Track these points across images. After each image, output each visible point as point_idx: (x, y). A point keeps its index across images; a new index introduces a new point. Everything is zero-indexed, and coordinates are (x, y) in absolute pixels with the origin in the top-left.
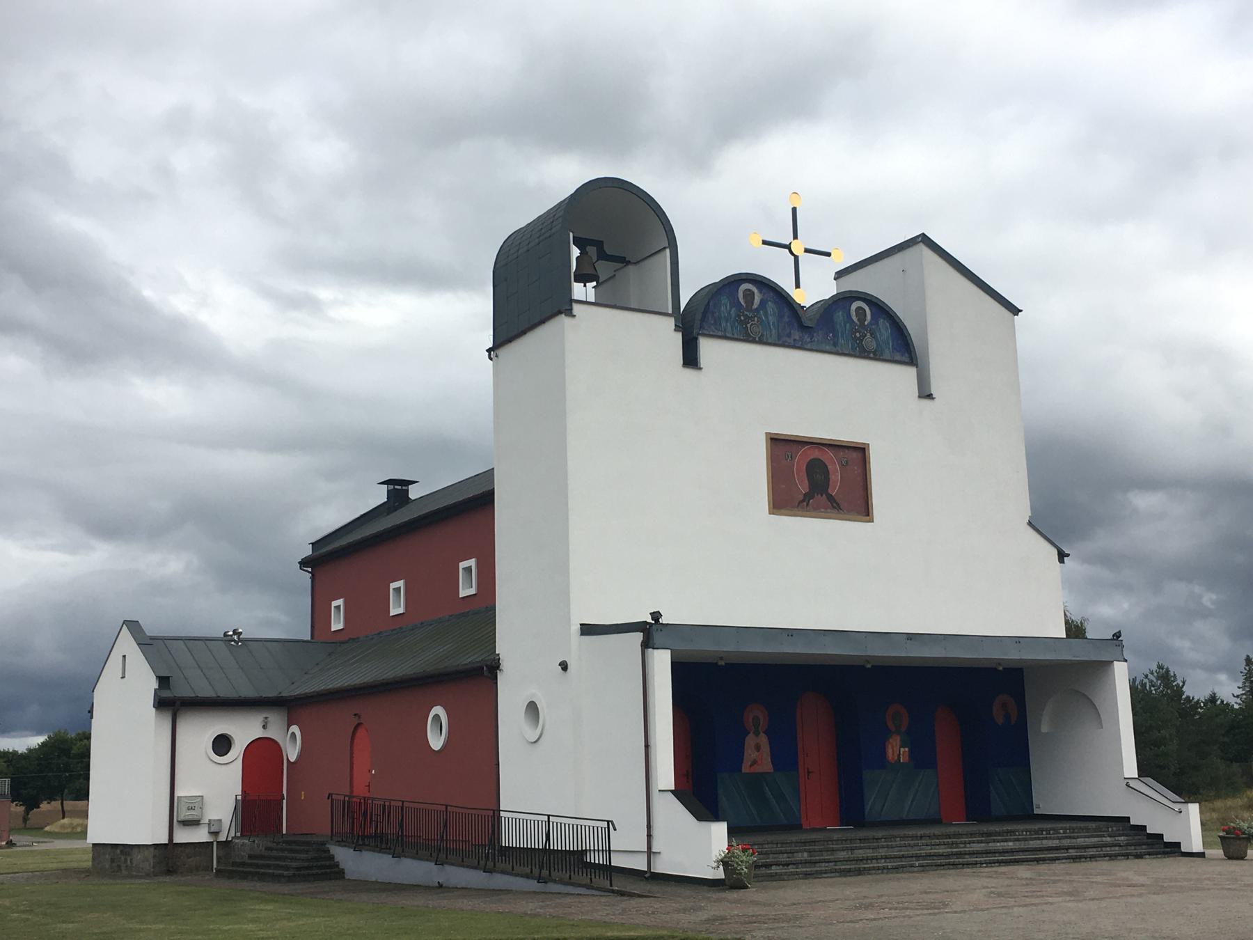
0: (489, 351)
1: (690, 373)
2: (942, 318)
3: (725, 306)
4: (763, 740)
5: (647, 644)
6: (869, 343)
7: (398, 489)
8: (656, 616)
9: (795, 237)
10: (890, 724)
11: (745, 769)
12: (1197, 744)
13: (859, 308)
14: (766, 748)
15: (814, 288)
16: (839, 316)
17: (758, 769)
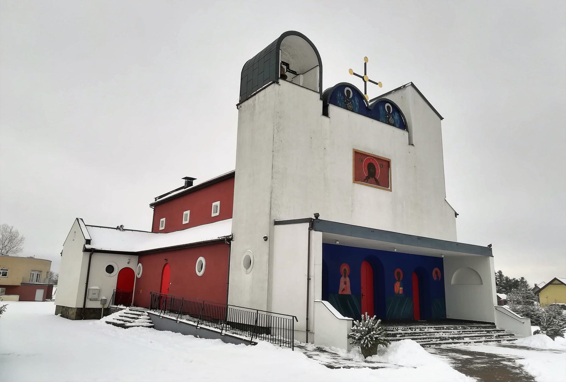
0: (237, 105)
1: (324, 118)
4: (348, 279)
5: (311, 228)
6: (391, 120)
7: (189, 181)
8: (317, 215)
9: (365, 74)
11: (340, 292)
12: (32, 286)
14: (348, 284)
15: (372, 94)
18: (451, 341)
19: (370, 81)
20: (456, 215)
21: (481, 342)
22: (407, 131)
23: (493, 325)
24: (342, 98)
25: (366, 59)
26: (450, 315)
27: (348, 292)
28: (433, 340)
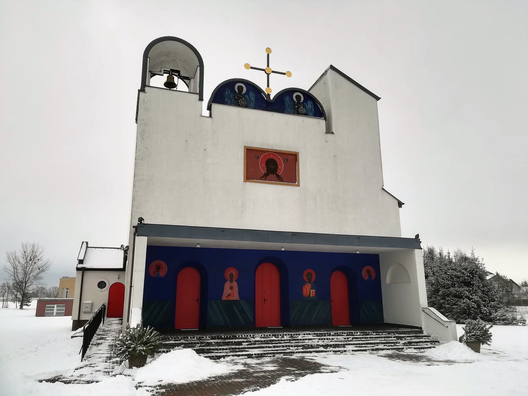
2: (330, 98)
3: (227, 92)
4: (235, 284)
9: (268, 66)
10: (305, 278)
11: (224, 298)
13: (239, 87)
15: (275, 87)
16: (287, 99)
17: (231, 298)
18: (321, 349)
19: (273, 72)
20: (400, 204)
21: (366, 350)
22: (325, 119)
23: (420, 330)
24: (232, 95)
25: (269, 50)
26: (388, 319)
27: (236, 297)
28: (291, 348)
